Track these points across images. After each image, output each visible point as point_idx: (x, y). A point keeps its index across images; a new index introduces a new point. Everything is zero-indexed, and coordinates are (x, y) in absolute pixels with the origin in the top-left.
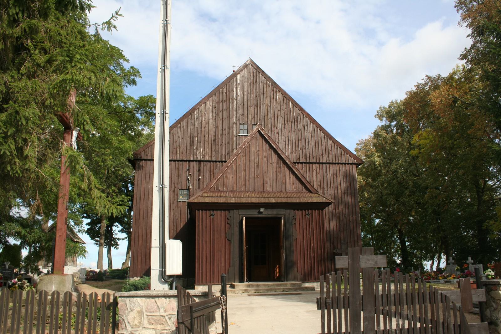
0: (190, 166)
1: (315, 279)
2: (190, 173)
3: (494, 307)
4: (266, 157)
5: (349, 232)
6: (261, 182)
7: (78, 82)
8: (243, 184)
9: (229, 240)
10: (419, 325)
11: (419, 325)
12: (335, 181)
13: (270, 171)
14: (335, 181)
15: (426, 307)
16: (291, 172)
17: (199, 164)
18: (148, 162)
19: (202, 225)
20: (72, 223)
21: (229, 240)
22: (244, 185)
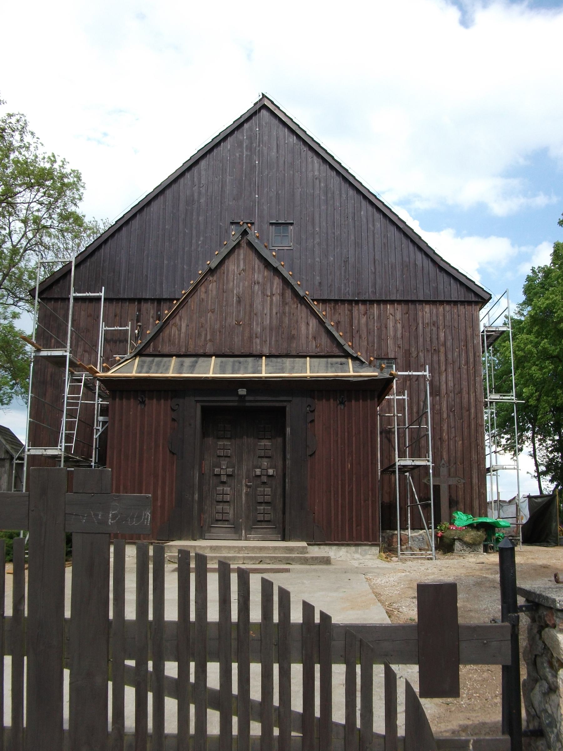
0: (139, 310)
1: (351, 539)
2: (139, 324)
3: (548, 683)
4: (258, 283)
5: (460, 442)
6: (247, 334)
7: (535, 309)
8: (208, 338)
9: (173, 454)
10: (256, 729)
11: (256, 729)
12: (434, 336)
13: (267, 310)
14: (434, 336)
15: (285, 675)
16: (311, 312)
17: (157, 306)
18: (60, 304)
19: (121, 420)
20: (508, 449)
21: (173, 454)
22: (210, 340)
